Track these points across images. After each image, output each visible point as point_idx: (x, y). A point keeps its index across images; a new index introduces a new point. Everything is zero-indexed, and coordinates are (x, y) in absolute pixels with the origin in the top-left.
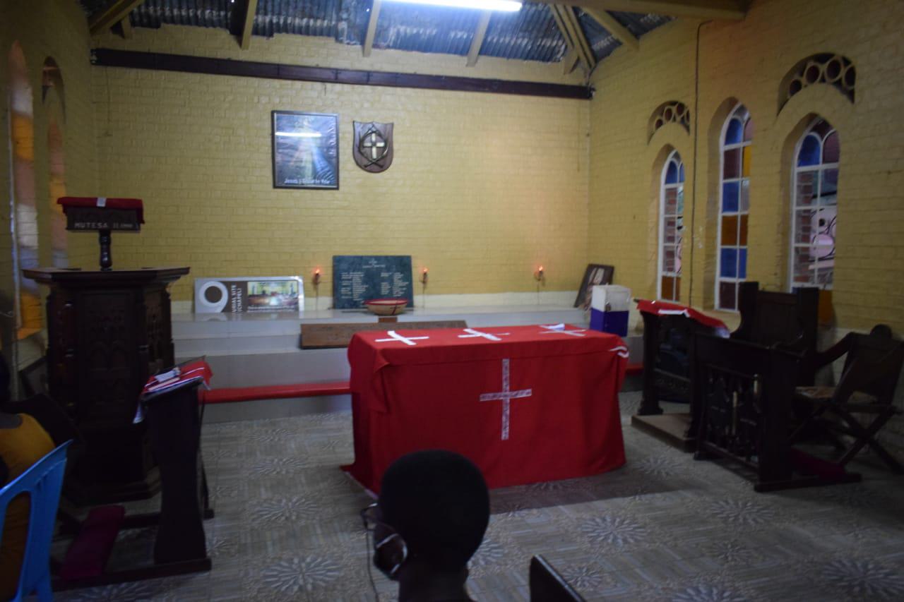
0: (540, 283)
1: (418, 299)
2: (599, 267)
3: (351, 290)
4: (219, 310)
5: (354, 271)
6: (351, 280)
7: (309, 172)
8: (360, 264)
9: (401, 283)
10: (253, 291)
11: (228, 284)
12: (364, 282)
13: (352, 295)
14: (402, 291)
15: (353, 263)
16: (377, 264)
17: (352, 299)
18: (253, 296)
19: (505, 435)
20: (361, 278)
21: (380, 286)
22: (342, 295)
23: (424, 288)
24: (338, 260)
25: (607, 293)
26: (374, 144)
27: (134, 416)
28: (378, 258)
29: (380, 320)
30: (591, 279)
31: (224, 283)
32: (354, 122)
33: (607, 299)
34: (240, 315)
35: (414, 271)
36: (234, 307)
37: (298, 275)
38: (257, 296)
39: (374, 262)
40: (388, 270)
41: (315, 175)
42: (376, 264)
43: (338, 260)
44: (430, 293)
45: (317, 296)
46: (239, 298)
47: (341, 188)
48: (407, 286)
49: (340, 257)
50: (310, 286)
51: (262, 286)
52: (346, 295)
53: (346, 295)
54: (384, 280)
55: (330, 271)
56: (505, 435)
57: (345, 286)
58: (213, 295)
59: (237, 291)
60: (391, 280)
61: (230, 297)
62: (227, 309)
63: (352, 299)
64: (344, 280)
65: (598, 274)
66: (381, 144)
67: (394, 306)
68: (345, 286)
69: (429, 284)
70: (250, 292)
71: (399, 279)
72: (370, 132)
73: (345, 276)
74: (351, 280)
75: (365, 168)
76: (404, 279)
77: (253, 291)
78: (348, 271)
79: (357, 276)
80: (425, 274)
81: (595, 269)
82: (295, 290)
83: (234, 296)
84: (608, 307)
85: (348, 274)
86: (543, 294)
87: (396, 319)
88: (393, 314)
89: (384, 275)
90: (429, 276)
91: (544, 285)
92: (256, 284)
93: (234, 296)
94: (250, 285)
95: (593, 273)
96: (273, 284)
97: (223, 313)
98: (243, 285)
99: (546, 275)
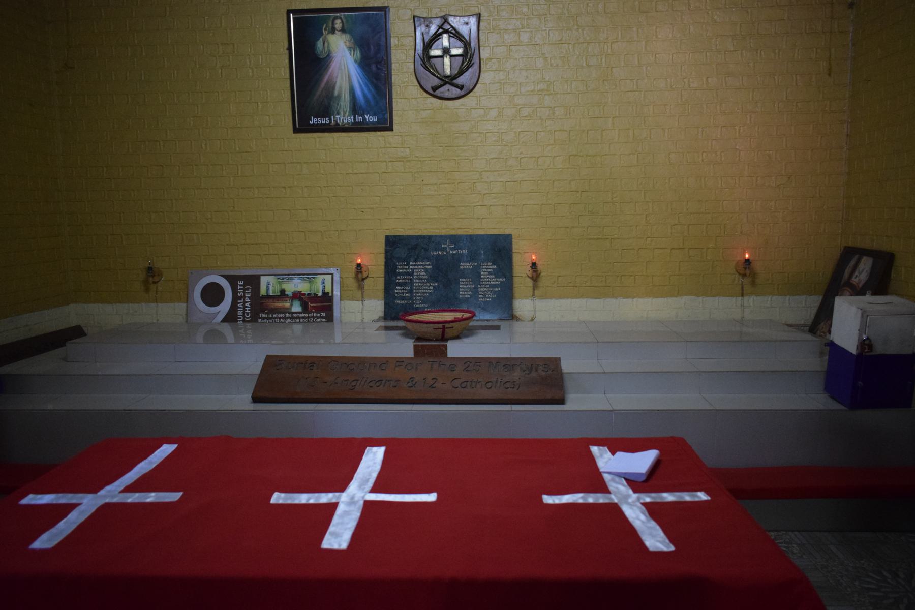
0: (747, 281)
1: (523, 306)
2: (864, 252)
3: (411, 291)
4: (221, 317)
5: (416, 261)
6: (411, 274)
7: (345, 103)
8: (426, 250)
9: (493, 280)
10: (268, 290)
11: (232, 279)
12: (432, 277)
13: (411, 298)
14: (494, 293)
15: (415, 247)
16: (455, 249)
17: (411, 305)
18: (268, 297)
19: (702, 496)
20: (426, 270)
21: (458, 283)
22: (396, 298)
23: (535, 287)
24: (392, 243)
25: (864, 314)
26: (446, 51)
27: (745, 255)
28: (455, 239)
29: (417, 350)
30: (846, 275)
31: (226, 277)
32: (414, 17)
33: (862, 330)
34: (249, 325)
35: (516, 258)
36: (240, 313)
37: (334, 266)
38: (273, 297)
39: (448, 245)
40: (472, 257)
41: (355, 109)
42: (452, 249)
43: (392, 243)
44: (544, 297)
45: (363, 299)
46: (247, 300)
47: (395, 127)
48: (501, 285)
49: (395, 237)
50: (352, 283)
51: (280, 283)
52: (403, 298)
53: (403, 298)
54: (463, 274)
55: (381, 260)
56: (702, 496)
57: (399, 284)
58: (212, 295)
59: (244, 289)
60: (476, 275)
61: (235, 299)
62: (231, 317)
63: (411, 305)
64: (400, 274)
65: (861, 266)
66: (459, 51)
67: (440, 326)
68: (399, 284)
69: (544, 281)
70: (263, 291)
71: (490, 273)
72: (441, 30)
73: (401, 267)
74: (411, 274)
75: (433, 92)
76: (496, 274)
77: (268, 290)
78: (407, 261)
79: (421, 268)
80: (534, 265)
81: (857, 257)
82: (328, 289)
83: (240, 298)
84: (866, 344)
85: (408, 264)
86: (751, 301)
87: (443, 351)
88: (444, 338)
89: (465, 266)
90: (540, 267)
91: (753, 283)
92: (272, 279)
93: (240, 298)
94: (264, 280)
95: (852, 263)
96: (296, 280)
97: (226, 324)
98: (253, 281)
99: (758, 266)
